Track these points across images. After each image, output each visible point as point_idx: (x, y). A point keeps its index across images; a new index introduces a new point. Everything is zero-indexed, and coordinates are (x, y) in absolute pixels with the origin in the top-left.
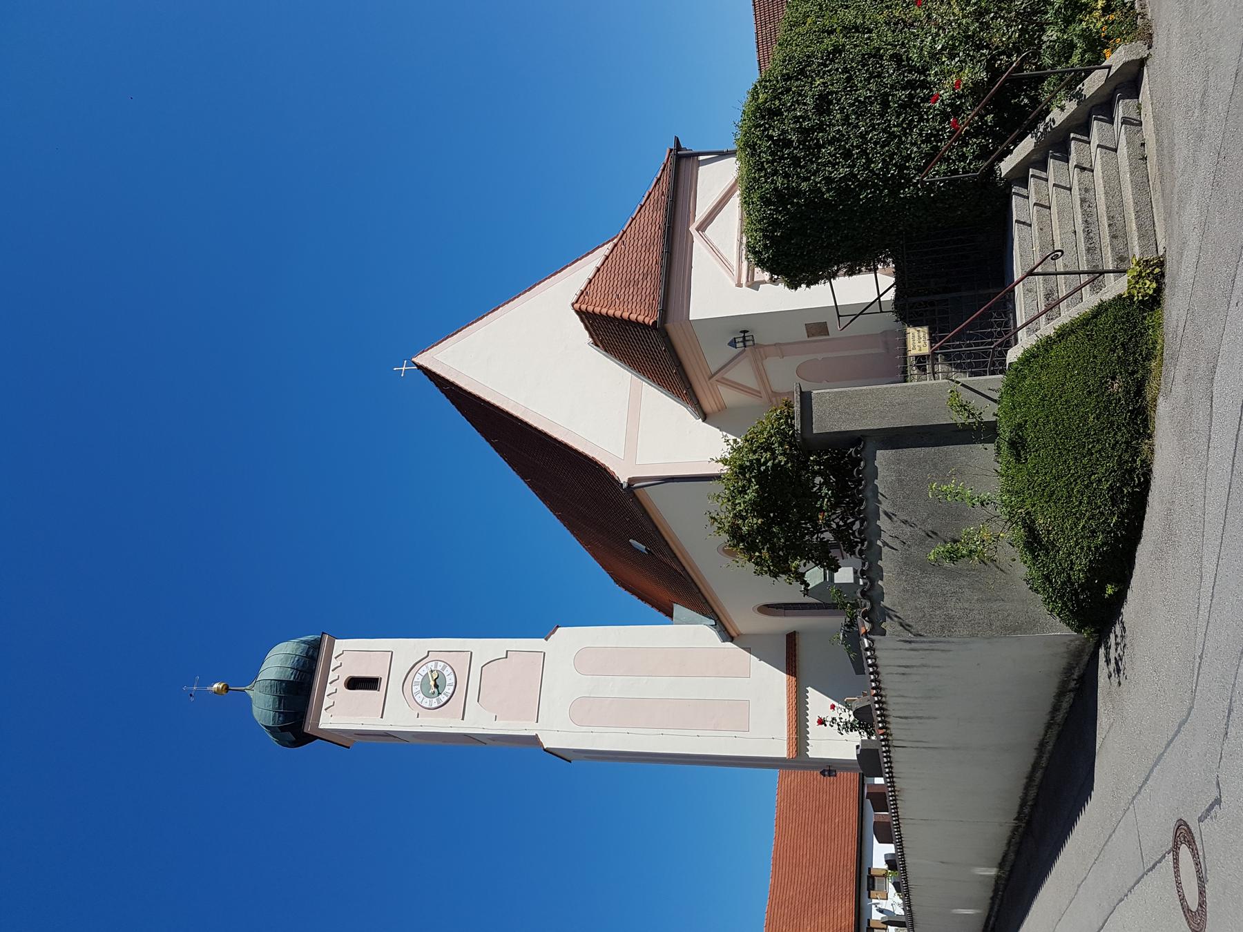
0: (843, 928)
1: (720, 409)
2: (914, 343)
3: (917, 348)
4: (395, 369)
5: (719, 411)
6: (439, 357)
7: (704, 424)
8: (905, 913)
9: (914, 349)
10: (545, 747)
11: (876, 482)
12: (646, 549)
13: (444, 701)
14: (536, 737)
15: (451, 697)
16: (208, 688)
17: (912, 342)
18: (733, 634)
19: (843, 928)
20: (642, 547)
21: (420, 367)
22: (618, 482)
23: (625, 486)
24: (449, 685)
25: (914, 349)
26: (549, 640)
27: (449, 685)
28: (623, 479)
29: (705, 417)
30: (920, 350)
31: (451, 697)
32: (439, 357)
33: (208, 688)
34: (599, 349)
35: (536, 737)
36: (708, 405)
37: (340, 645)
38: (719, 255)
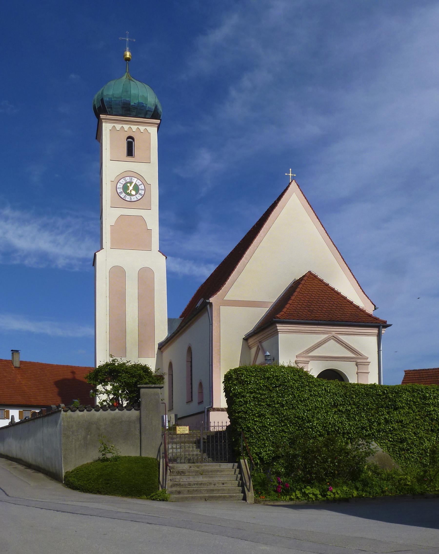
0: (30, 399)
1: (250, 346)
2: (182, 428)
3: (179, 429)
4: (290, 170)
5: (249, 346)
6: (294, 195)
7: (242, 340)
8: (239, 460)
9: (179, 428)
10: (96, 254)
11: (85, 411)
12: (198, 307)
13: (121, 196)
14: (102, 248)
15: (124, 199)
16: (128, 48)
17: (183, 427)
18: (162, 350)
19: (30, 399)
20: (199, 305)
21: (290, 184)
22: (210, 297)
23: (207, 301)
24: (131, 198)
25: (179, 428)
26: (159, 252)
27: (131, 198)
28: (211, 300)
29: (246, 339)
30: (178, 430)
31: (124, 199)
32: (294, 195)
33: (128, 48)
34: (292, 283)
35: (102, 248)
36: (251, 341)
37: (153, 131)
38: (344, 345)
